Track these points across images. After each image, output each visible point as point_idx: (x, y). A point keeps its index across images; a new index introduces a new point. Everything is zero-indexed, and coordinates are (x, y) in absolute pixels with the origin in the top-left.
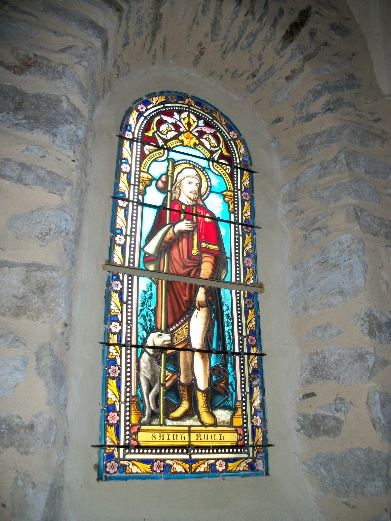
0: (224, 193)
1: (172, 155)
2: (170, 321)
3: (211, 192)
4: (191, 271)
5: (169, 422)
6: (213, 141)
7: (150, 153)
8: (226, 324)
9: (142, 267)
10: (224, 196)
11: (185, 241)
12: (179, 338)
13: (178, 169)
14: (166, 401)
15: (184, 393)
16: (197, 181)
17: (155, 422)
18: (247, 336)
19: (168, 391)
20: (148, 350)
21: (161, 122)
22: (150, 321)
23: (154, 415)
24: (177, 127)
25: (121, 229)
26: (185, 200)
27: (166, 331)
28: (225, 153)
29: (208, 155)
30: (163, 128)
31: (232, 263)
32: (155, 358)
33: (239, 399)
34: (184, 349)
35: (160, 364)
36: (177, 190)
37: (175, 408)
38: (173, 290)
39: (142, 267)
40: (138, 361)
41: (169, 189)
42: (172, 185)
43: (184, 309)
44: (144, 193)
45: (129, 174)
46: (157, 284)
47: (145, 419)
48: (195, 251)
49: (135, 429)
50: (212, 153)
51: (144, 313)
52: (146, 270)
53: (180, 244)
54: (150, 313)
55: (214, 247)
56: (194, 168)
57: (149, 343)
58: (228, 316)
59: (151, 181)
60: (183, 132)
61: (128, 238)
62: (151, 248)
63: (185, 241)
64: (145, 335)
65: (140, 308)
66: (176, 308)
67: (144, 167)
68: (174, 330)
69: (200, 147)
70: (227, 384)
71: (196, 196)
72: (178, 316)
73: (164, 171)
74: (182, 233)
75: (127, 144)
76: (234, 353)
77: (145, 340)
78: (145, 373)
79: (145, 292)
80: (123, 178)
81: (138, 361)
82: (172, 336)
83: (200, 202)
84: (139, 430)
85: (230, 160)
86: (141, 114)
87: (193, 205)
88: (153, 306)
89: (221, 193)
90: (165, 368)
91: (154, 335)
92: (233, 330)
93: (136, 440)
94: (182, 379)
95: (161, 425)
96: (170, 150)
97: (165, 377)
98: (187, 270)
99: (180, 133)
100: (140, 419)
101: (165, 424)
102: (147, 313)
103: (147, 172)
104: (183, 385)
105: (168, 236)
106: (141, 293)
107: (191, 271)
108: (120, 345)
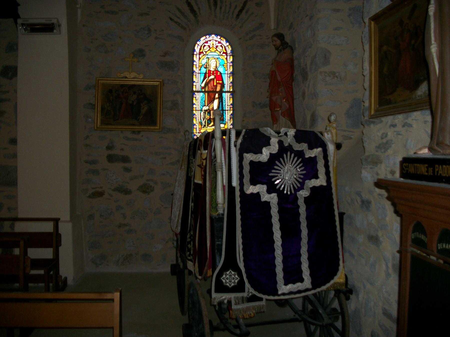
0: (224, 65)
1: (208, 56)
2: (209, 103)
3: (220, 65)
4: (214, 90)
5: (208, 127)
6: (221, 48)
7: (202, 57)
8: (223, 103)
9: (201, 90)
10: (224, 66)
11: (212, 82)
12: (211, 107)
13: (210, 60)
14: (207, 122)
15: (212, 120)
16: (216, 63)
17: (205, 127)
18: (230, 105)
19: (208, 120)
20: (203, 111)
21: (205, 46)
22: (203, 104)
23: (205, 126)
24: (209, 46)
25: (195, 81)
26: (212, 69)
27: (207, 106)
28: (225, 51)
29: (219, 53)
30: (205, 48)
31: (226, 86)
32: (205, 113)
33: (227, 121)
34: (212, 110)
35: (206, 114)
36: (210, 67)
37: (210, 124)
38: (209, 96)
39: (201, 90)
40: (200, 114)
41: (207, 67)
42: (208, 65)
43: (212, 100)
44: (200, 70)
45: (196, 65)
46: (205, 94)
47: (202, 127)
48: (215, 84)
49: (200, 129)
50: (220, 52)
51: (202, 102)
52: (202, 91)
53: (211, 83)
54: (203, 102)
55: (221, 82)
56: (215, 59)
57: (203, 109)
58: (224, 100)
59: (202, 66)
60: (211, 48)
61: (197, 83)
62: (203, 85)
63: (212, 82)
64: (202, 107)
65: (201, 101)
66: (210, 100)
67: (200, 62)
68: (209, 106)
69: (217, 51)
70: (223, 118)
71: (215, 68)
72: (211, 102)
73: (206, 62)
74: (211, 79)
75: (195, 56)
76: (226, 110)
77: (202, 109)
78: (202, 117)
79: (202, 97)
80: (195, 66)
81: (200, 114)
82: (209, 107)
83: (216, 69)
84: (201, 129)
85: (226, 53)
86: (198, 45)
87: (214, 71)
88: (204, 100)
89: (223, 65)
90: (207, 115)
91: (204, 107)
92: (225, 104)
93: (201, 131)
94: (212, 117)
95: (206, 128)
96: (207, 55)
97: (207, 117)
98: (213, 89)
99: (210, 48)
100: (201, 127)
101: (207, 128)
102: (202, 102)
103: (201, 63)
104: (212, 119)
105: (208, 81)
106: (201, 97)
107: (214, 90)
108: (196, 110)
